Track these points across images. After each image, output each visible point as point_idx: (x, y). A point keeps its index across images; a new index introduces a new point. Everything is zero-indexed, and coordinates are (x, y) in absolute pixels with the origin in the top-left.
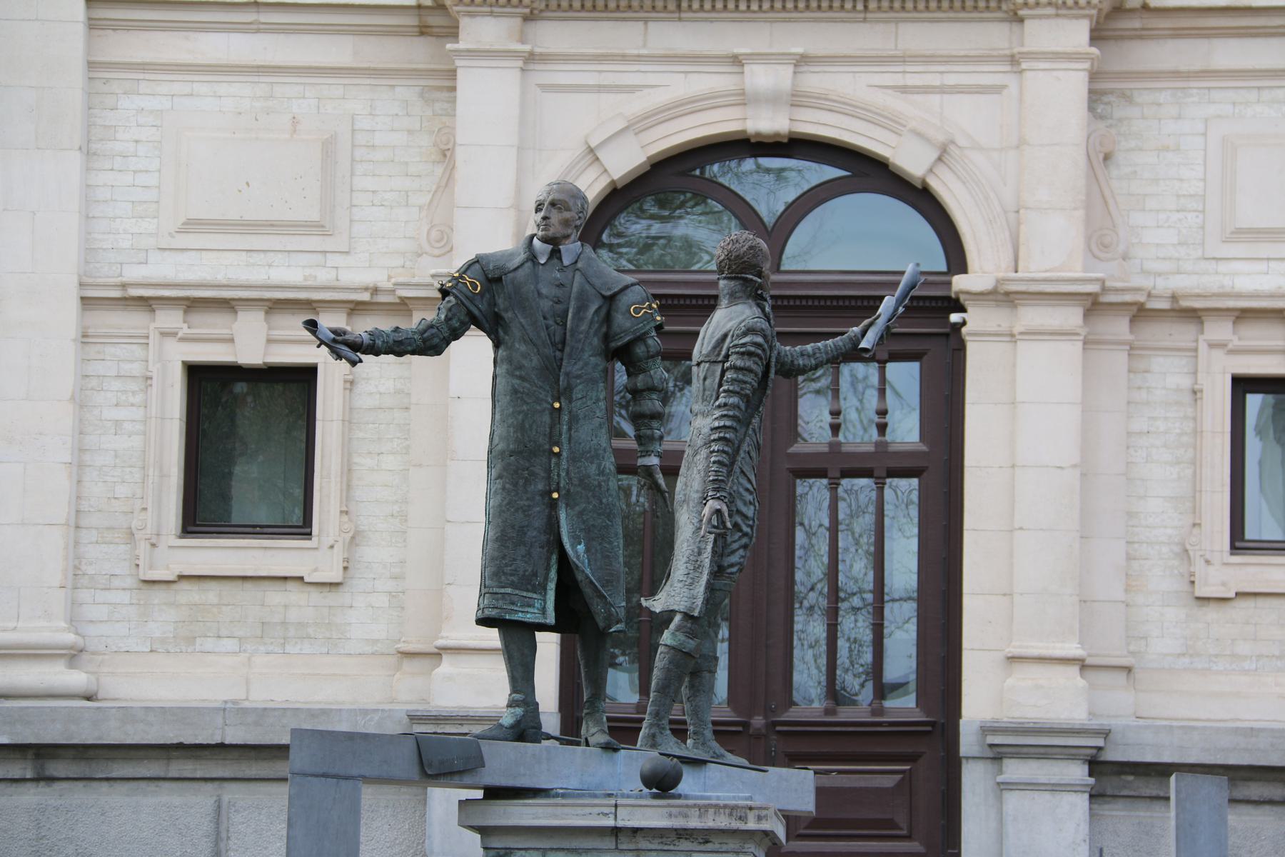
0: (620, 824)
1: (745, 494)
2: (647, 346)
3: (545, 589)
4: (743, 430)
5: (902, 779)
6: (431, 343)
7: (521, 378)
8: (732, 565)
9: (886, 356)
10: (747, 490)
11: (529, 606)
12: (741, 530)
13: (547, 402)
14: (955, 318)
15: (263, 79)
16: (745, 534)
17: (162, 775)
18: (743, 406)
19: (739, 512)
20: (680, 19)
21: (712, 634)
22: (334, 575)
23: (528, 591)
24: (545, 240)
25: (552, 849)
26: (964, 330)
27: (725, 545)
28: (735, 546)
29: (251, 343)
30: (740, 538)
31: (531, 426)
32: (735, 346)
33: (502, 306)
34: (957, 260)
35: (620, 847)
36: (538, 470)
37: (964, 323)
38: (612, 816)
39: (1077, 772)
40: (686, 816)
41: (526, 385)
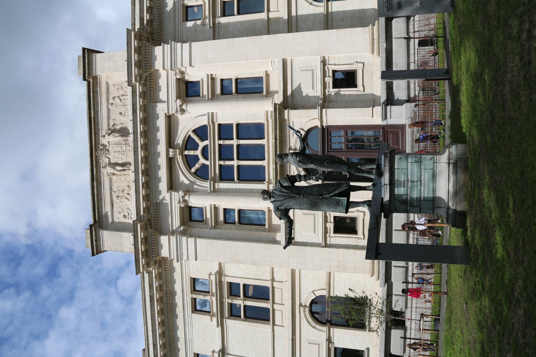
0: (394, 41)
6: (290, 223)
22: (363, 213)
39: (388, 107)
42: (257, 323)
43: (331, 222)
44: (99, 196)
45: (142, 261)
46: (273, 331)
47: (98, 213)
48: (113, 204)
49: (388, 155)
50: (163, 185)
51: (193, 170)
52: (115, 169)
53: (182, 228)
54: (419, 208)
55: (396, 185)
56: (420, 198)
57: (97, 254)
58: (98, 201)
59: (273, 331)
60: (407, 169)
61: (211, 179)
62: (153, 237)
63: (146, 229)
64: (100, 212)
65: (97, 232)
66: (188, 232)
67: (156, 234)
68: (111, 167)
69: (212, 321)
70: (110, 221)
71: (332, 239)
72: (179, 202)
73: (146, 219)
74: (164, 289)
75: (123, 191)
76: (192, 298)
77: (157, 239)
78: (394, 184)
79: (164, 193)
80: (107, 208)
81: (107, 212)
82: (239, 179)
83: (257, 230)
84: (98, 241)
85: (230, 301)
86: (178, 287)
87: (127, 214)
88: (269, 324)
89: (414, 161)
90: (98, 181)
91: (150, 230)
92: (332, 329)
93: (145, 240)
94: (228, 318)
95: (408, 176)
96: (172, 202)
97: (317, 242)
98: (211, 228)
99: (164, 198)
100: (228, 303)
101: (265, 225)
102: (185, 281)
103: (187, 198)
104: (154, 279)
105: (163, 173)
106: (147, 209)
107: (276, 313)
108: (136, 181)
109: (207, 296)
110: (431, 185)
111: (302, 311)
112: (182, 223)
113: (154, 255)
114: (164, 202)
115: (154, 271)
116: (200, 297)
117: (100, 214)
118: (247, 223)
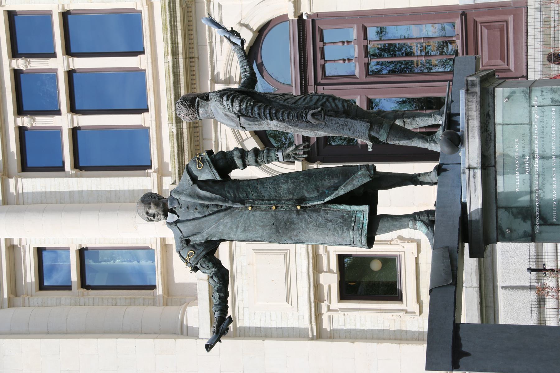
0: (479, 165)
1: (306, 101)
2: (219, 159)
3: (350, 211)
4: (274, 103)
5: (484, 26)
6: (222, 277)
7: (237, 227)
8: (343, 106)
9: (322, 43)
10: (304, 100)
11: (360, 220)
12: (325, 102)
13: (248, 214)
14: (305, 17)
15: (235, 276)
16: (327, 100)
17: (493, 309)
18: (260, 104)
19: (316, 103)
20: (202, 127)
21: (384, 114)
22: (414, 245)
23: (351, 221)
24: (166, 215)
25: (496, 203)
26: (309, 13)
27: (333, 110)
28: (333, 105)
29: (331, 281)
30: (329, 103)
31: (262, 222)
32: (229, 110)
33: (201, 239)
34: (283, 19)
35: (493, 164)
36: (286, 217)
37: (307, 13)
38: (476, 170)
40: (473, 127)
41: (240, 225)
43: (330, 271)
55: (499, 169)
60: (530, 124)
71: (335, 316)
89: (548, 102)
95: (531, 142)
97: (296, 325)
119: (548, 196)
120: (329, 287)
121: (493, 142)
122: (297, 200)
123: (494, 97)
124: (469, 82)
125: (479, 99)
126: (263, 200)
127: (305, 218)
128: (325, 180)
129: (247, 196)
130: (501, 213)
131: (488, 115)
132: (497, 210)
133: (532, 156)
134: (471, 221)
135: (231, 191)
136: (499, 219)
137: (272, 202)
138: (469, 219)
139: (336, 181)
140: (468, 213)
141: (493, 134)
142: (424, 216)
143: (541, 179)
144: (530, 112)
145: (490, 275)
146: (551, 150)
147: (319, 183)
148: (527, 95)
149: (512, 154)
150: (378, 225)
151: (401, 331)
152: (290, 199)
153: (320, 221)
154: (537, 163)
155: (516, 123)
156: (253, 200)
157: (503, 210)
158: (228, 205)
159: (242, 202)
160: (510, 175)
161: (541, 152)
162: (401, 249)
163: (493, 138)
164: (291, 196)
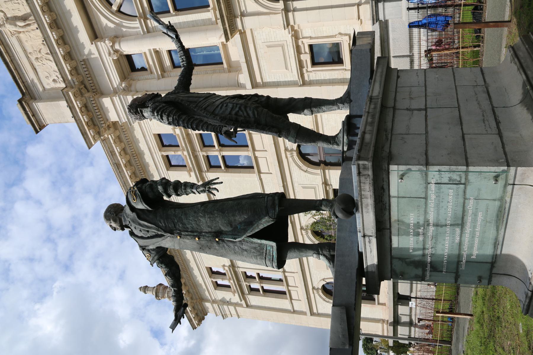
10: (221, 108)
11: (270, 252)
12: (238, 111)
16: (240, 108)
23: (263, 253)
29: (306, 58)
30: (242, 111)
42: (240, 173)
43: (306, 53)
44: (14, 62)
45: (90, 133)
46: (261, 179)
47: (23, 82)
48: (35, 69)
49: (370, 172)
50: (83, 36)
51: (115, 8)
52: (16, 25)
53: (123, 85)
54: (454, 275)
55: (394, 230)
56: (459, 256)
57: (41, 129)
58: (16, 69)
59: (261, 179)
60: (426, 198)
61: (141, 17)
62: (93, 102)
63: (82, 94)
64: (24, 81)
65: (31, 106)
66: (133, 88)
67: (96, 97)
68: (10, 24)
69: (190, 176)
70: (41, 89)
71: (311, 74)
72: (110, 54)
73: (76, 83)
74: (129, 151)
75: (40, 52)
76: (162, 156)
77: (99, 103)
78: (390, 229)
79: (88, 47)
80: (30, 75)
81: (33, 80)
82: (176, 9)
83: (214, 72)
84: (36, 116)
85: (205, 154)
86: (143, 146)
87: (56, 78)
88: (254, 173)
90: (5, 44)
91: (87, 95)
92: (327, 171)
93: (86, 108)
94: (208, 171)
95: (426, 212)
96: (101, 55)
97: (292, 79)
98: (159, 79)
99: (90, 50)
100: (203, 155)
101: (222, 63)
102: (148, 139)
103: (117, 47)
104: (113, 145)
105: (77, 20)
106: (75, 70)
107: (260, 160)
108: (46, 40)
109: (178, 151)
110: (491, 233)
111: (289, 156)
112: (123, 77)
113: (102, 122)
114: (92, 56)
115: (110, 136)
116: (171, 153)
117: (26, 84)
118: (201, 63)
119: (439, 252)
120: (306, 61)
121: (388, 211)
122: (215, 232)
123: (389, 173)
124: (361, 166)
125: (372, 182)
126: (187, 231)
127: (224, 246)
128: (237, 216)
129: (175, 227)
130: (395, 262)
131: (383, 188)
132: (391, 259)
133: (427, 223)
134: (367, 272)
135: (162, 221)
136: (393, 266)
137: (195, 234)
138: (365, 271)
139: (246, 217)
140: (365, 267)
141: (387, 205)
142: (326, 251)
143: (434, 241)
144: (426, 188)
145: (387, 51)
146: (446, 220)
147: (232, 218)
148: (424, 174)
149: (406, 221)
150: (287, 254)
151: (344, 79)
152: (209, 232)
153: (237, 250)
154: (431, 229)
155: (412, 196)
156: (180, 231)
157: (397, 260)
158: (160, 233)
159: (172, 232)
160: (404, 237)
161: (435, 221)
162: (341, 39)
163: (388, 207)
164: (210, 230)
